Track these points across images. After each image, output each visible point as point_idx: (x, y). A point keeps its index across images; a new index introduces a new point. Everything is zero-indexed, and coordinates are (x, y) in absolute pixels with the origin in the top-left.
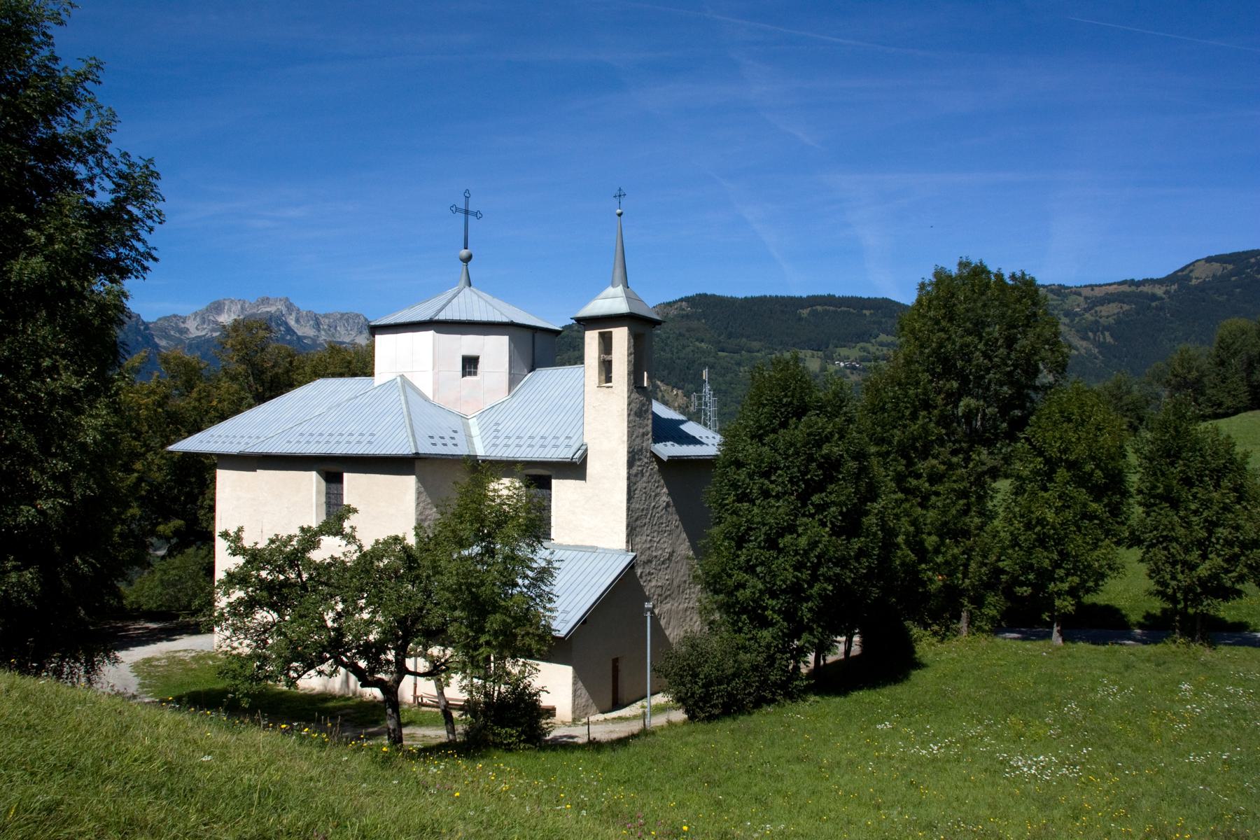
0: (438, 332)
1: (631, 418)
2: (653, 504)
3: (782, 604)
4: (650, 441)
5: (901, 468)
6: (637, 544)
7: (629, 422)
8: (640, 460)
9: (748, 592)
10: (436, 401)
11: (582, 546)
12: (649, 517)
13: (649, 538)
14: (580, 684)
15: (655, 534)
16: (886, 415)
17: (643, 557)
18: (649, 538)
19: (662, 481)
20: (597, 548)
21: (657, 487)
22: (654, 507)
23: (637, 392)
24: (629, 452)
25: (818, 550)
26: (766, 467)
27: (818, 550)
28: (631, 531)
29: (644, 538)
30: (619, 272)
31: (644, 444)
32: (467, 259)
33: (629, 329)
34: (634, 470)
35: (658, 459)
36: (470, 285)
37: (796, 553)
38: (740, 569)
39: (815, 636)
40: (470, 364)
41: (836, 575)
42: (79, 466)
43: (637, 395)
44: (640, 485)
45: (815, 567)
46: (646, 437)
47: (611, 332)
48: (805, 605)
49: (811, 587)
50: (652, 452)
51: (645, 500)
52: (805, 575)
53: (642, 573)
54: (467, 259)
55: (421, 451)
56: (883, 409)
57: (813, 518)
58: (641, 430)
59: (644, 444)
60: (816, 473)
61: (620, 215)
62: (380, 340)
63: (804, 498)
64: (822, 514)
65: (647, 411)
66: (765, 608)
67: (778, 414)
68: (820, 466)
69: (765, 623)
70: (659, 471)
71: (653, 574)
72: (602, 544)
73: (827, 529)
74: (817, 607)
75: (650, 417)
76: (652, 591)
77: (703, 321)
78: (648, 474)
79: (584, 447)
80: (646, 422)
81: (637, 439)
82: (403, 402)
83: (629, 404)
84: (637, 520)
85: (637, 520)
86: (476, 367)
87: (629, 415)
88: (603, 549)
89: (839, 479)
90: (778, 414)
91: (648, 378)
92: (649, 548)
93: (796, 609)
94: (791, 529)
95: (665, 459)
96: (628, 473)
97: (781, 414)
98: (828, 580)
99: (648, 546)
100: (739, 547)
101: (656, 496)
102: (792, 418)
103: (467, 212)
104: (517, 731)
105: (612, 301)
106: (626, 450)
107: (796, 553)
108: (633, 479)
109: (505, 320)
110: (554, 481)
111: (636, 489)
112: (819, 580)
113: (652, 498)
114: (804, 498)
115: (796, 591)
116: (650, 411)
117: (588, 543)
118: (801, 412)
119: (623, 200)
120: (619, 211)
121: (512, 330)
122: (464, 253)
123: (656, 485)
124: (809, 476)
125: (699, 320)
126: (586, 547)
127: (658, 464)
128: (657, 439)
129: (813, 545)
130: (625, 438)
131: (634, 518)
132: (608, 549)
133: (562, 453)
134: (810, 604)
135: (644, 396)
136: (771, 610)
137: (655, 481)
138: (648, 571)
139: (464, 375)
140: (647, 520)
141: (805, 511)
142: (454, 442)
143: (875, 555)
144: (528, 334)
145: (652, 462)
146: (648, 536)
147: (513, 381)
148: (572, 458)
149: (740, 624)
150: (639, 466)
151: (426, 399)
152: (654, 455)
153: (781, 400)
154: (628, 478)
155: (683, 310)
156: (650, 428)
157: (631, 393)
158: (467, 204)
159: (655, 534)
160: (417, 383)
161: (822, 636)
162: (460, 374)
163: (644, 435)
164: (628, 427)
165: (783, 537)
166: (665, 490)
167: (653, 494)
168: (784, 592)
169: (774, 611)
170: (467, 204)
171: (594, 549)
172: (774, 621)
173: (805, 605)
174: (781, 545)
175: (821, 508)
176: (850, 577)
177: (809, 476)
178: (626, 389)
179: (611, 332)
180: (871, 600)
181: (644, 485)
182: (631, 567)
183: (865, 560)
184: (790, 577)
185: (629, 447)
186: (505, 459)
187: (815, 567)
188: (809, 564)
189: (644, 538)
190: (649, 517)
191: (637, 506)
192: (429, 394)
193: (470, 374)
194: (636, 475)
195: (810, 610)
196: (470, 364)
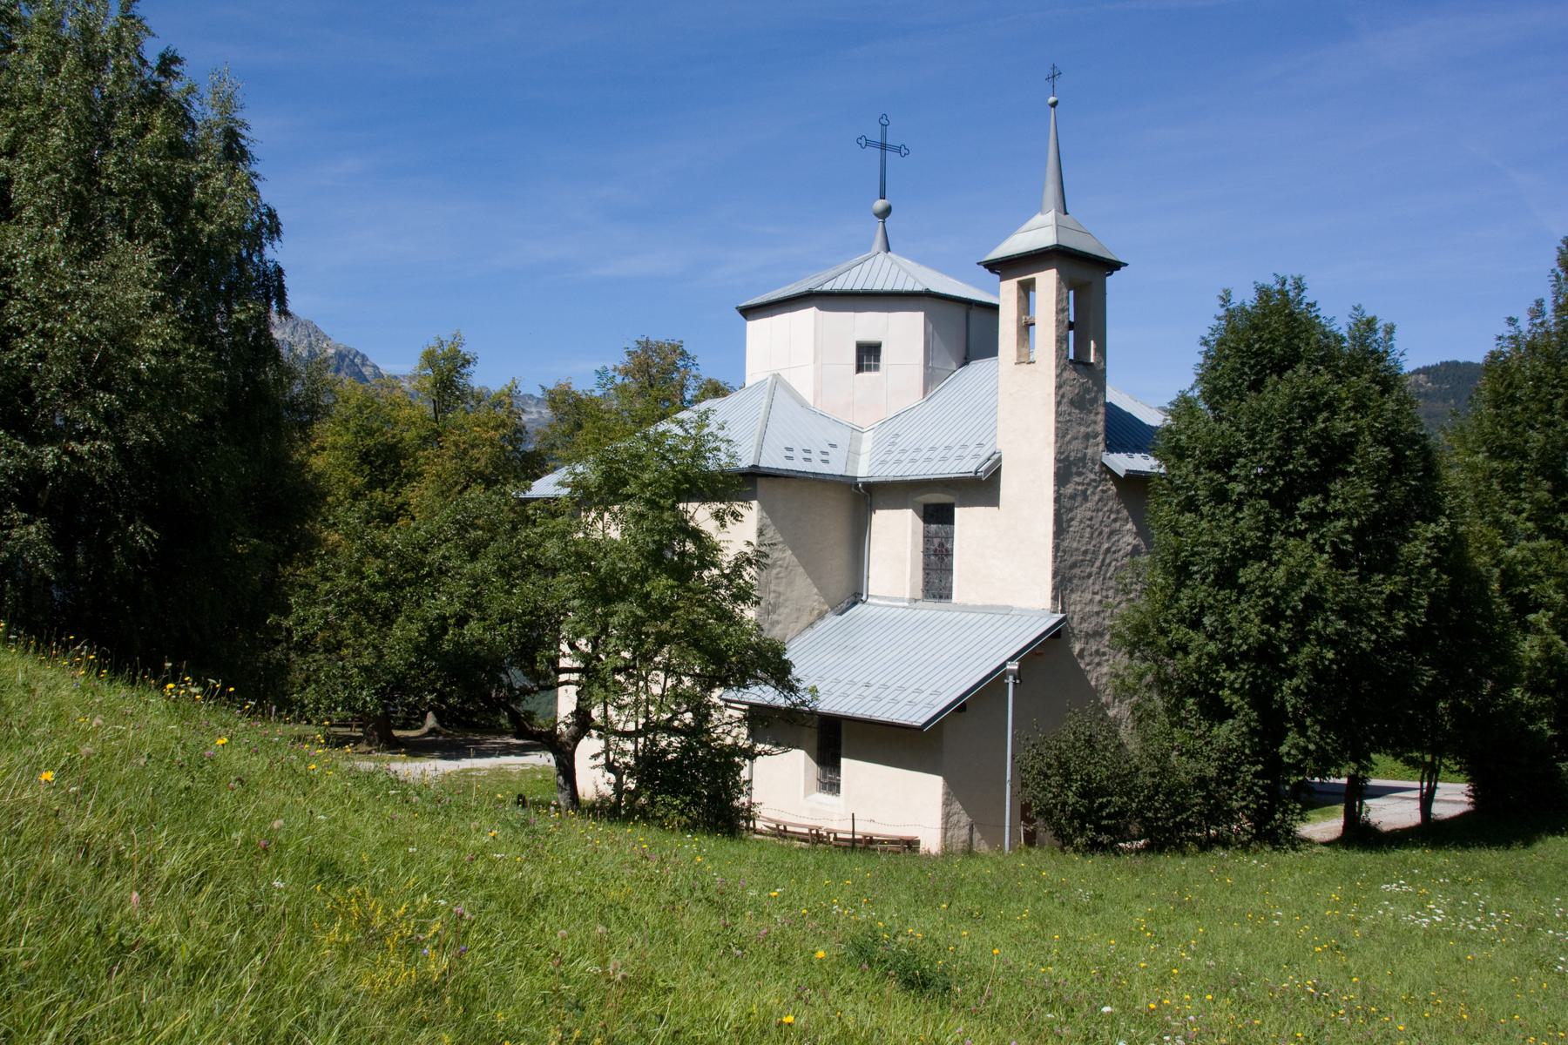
0: (821, 309)
1: (1063, 408)
2: (1106, 546)
3: (1244, 680)
4: (1102, 446)
5: (1542, 495)
6: (1075, 603)
7: (1058, 414)
8: (1080, 474)
9: (1192, 658)
10: (818, 408)
11: (992, 607)
12: (1098, 564)
13: (1098, 598)
14: (957, 806)
15: (1111, 593)
16: (1518, 408)
17: (1085, 625)
18: (1098, 598)
19: (1125, 513)
20: (1012, 609)
21: (1115, 520)
22: (1108, 550)
23: (1075, 370)
24: (1057, 460)
25: (1306, 589)
26: (1219, 453)
27: (1306, 589)
28: (1061, 582)
29: (1088, 596)
30: (1051, 190)
31: (1090, 452)
32: (887, 212)
33: (1059, 272)
34: (1069, 489)
35: (1114, 476)
36: (888, 249)
37: (1266, 594)
38: (1182, 621)
39: (1308, 739)
40: (868, 354)
41: (1338, 632)
42: (133, 405)
43: (1073, 375)
44: (1081, 513)
45: (1301, 619)
46: (1092, 441)
47: (1034, 279)
48: (1287, 683)
49: (1294, 650)
50: (1103, 465)
51: (1091, 538)
52: (1285, 630)
53: (1082, 650)
54: (887, 212)
55: (763, 464)
56: (1513, 400)
57: (1304, 539)
58: (1083, 429)
59: (1090, 452)
60: (1301, 460)
61: (1054, 105)
62: (757, 329)
63: (1284, 501)
64: (1318, 531)
65: (1094, 401)
66: (1221, 686)
67: (1246, 370)
68: (1313, 452)
69: (1216, 711)
70: (1117, 494)
71: (1104, 654)
72: (1019, 603)
73: (1326, 556)
74: (1307, 686)
75: (1102, 410)
76: (1104, 680)
77: (1452, 401)
78: (1096, 498)
79: (996, 456)
80: (1092, 417)
81: (1075, 442)
82: (764, 405)
83: (1059, 387)
84: (1073, 566)
85: (1073, 566)
86: (877, 359)
87: (1058, 404)
88: (1022, 610)
89: (1349, 474)
90: (1246, 370)
91: (1096, 350)
92: (1098, 614)
93: (1272, 690)
94: (1261, 552)
95: (1122, 474)
96: (1057, 492)
97: (1251, 368)
98: (1324, 641)
99: (1096, 609)
100: (1180, 585)
101: (1112, 533)
102: (1271, 374)
103: (883, 146)
104: (683, 801)
105: (1038, 233)
106: (1053, 456)
107: (1266, 594)
108: (1067, 503)
109: (918, 288)
110: (957, 511)
111: (1072, 519)
112: (1309, 640)
113: (1105, 535)
114: (1284, 501)
115: (1266, 655)
116: (1101, 402)
117: (1000, 602)
118: (1282, 366)
119: (1058, 82)
120: (1052, 99)
121: (927, 302)
122: (879, 205)
123: (1113, 516)
124: (1291, 467)
125: (1445, 400)
126: (998, 607)
127: (1116, 484)
128: (1111, 448)
129: (1296, 580)
130: (1052, 438)
131: (1068, 563)
132: (1026, 610)
133: (965, 465)
134: (1296, 681)
135: (1089, 377)
136: (1230, 688)
137: (1111, 511)
138: (1094, 648)
139: (860, 369)
140: (1095, 570)
141: (1288, 527)
142: (825, 457)
143: (1422, 607)
144: (958, 312)
145: (1105, 480)
146: (1094, 593)
147: (932, 379)
148: (976, 472)
149: (1183, 713)
150: (1079, 484)
151: (803, 404)
152: (1109, 471)
153: (1249, 346)
154: (1057, 500)
155: (1421, 386)
156: (1100, 427)
157: (1064, 370)
158: (884, 134)
159: (1111, 593)
160: (795, 384)
161: (1322, 738)
162: (853, 367)
163: (1087, 437)
164: (1057, 421)
165: (1245, 565)
166: (1130, 526)
167: (1107, 530)
168: (1244, 656)
169: (1235, 691)
170: (884, 134)
171: (1007, 610)
172: (1234, 707)
173: (1287, 683)
174: (1242, 580)
175: (1318, 518)
176: (1368, 640)
177: (1291, 467)
178: (1053, 364)
179: (1034, 279)
180: (1420, 686)
181: (1089, 514)
182: (1056, 636)
183: (1402, 614)
184: (1255, 630)
185: (1059, 452)
186: (891, 479)
187: (1301, 619)
188: (1289, 612)
189: (1088, 596)
190: (1098, 564)
191: (1075, 545)
192: (808, 397)
193: (869, 369)
194: (1073, 497)
195: (1296, 691)
196: (868, 354)
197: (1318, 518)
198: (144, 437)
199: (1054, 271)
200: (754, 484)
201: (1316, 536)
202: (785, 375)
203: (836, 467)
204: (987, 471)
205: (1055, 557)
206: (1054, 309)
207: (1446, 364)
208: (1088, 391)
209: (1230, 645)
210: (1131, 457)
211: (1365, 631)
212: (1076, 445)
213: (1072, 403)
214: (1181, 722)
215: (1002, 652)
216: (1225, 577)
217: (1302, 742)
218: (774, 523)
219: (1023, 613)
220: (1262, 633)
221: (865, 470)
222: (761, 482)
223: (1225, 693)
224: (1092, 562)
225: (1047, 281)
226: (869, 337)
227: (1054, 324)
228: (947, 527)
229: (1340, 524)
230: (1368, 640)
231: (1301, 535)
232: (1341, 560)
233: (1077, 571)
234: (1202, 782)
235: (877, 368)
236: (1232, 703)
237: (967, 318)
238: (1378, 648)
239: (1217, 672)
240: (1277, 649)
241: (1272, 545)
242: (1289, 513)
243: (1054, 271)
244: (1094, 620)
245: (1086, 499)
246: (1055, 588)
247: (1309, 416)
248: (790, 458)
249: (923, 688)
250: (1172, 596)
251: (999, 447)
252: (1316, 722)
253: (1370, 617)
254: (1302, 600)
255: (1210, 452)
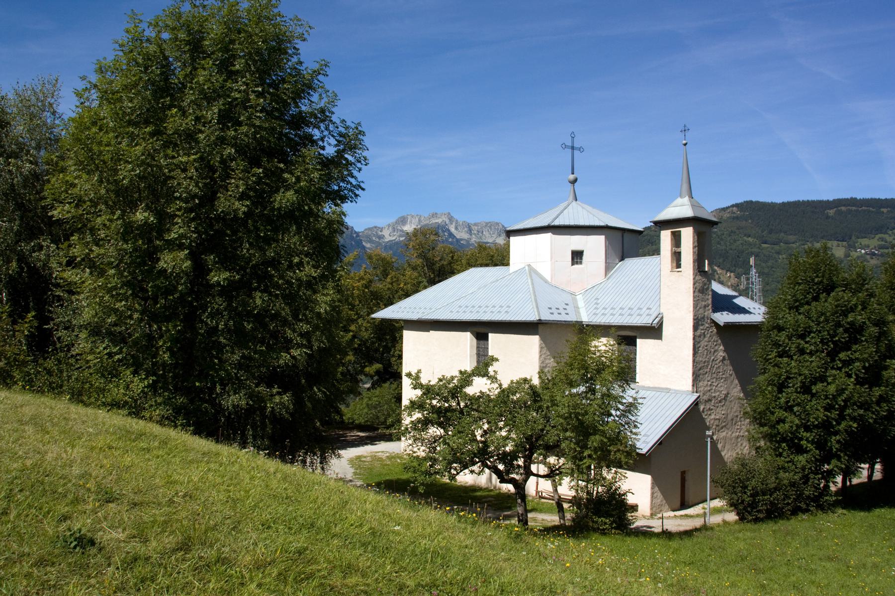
0: (554, 234)
1: (696, 294)
3: (814, 436)
4: (711, 311)
7: (694, 297)
8: (702, 325)
10: (554, 283)
11: (659, 388)
14: (656, 489)
15: (714, 380)
19: (720, 341)
22: (713, 360)
24: (694, 319)
25: (845, 396)
27: (845, 396)
29: (706, 383)
31: (706, 314)
33: (694, 228)
34: (698, 333)
35: (716, 325)
36: (576, 200)
37: (826, 397)
38: (781, 408)
39: (841, 462)
40: (577, 256)
41: (860, 415)
42: (316, 328)
43: (700, 277)
44: (703, 343)
45: (842, 409)
47: (680, 231)
49: (839, 424)
50: (711, 319)
52: (834, 414)
54: (575, 181)
58: (703, 303)
59: (706, 314)
60: (842, 336)
61: (685, 145)
63: (833, 355)
65: (708, 289)
66: (801, 439)
74: (844, 439)
75: (710, 293)
76: (712, 422)
79: (660, 316)
80: (707, 297)
83: (694, 284)
85: (699, 370)
86: (581, 258)
87: (694, 292)
91: (708, 264)
93: (826, 441)
94: (822, 379)
95: (722, 324)
96: (694, 335)
97: (814, 290)
98: (854, 419)
105: (681, 208)
107: (826, 397)
109: (602, 224)
110: (638, 341)
114: (833, 355)
115: (826, 426)
117: (663, 386)
118: (829, 288)
122: (572, 177)
125: (746, 221)
127: (716, 328)
128: (714, 311)
129: (841, 391)
130: (691, 309)
134: (838, 437)
139: (573, 264)
142: (566, 312)
144: (619, 234)
147: (608, 268)
149: (781, 450)
151: (546, 281)
152: (713, 322)
154: (694, 339)
156: (710, 302)
158: (573, 142)
162: (570, 263)
163: (705, 306)
164: (694, 301)
170: (573, 142)
171: (668, 390)
173: (834, 438)
175: (847, 363)
181: (706, 343)
182: (696, 404)
185: (694, 316)
188: (837, 406)
189: (706, 383)
191: (701, 359)
192: (548, 278)
193: (577, 263)
194: (700, 336)
195: (838, 442)
196: (577, 256)
197: (847, 363)
198: (322, 345)
199: (691, 228)
200: (537, 328)
201: (847, 370)
202: (533, 265)
203: (572, 318)
204: (658, 323)
205: (693, 366)
206: (692, 246)
207: (747, 202)
208: (705, 284)
209: (808, 421)
210: (722, 314)
211: (870, 415)
212: (701, 311)
213: (699, 291)
214: (780, 455)
215: (674, 412)
216: (806, 389)
217: (839, 464)
218: (546, 346)
219: (677, 392)
220: (824, 416)
221: (585, 318)
222: (540, 326)
223: (804, 442)
224: (707, 366)
225: (687, 234)
226: (578, 248)
227: (692, 254)
228: (631, 347)
229: (857, 364)
230: (872, 418)
231: (840, 369)
232: (859, 382)
233: (701, 371)
234: (793, 484)
235: (581, 263)
236: (807, 447)
237: (623, 236)
238: (875, 421)
239: (799, 433)
240: (831, 423)
241: (828, 374)
242: (833, 360)
243: (691, 228)
244: (708, 394)
245: (705, 337)
246: (693, 381)
247: (845, 314)
248: (552, 313)
249: (648, 434)
250: (776, 396)
251: (662, 311)
252: (846, 454)
253: (872, 407)
254: (843, 401)
255: (797, 330)
